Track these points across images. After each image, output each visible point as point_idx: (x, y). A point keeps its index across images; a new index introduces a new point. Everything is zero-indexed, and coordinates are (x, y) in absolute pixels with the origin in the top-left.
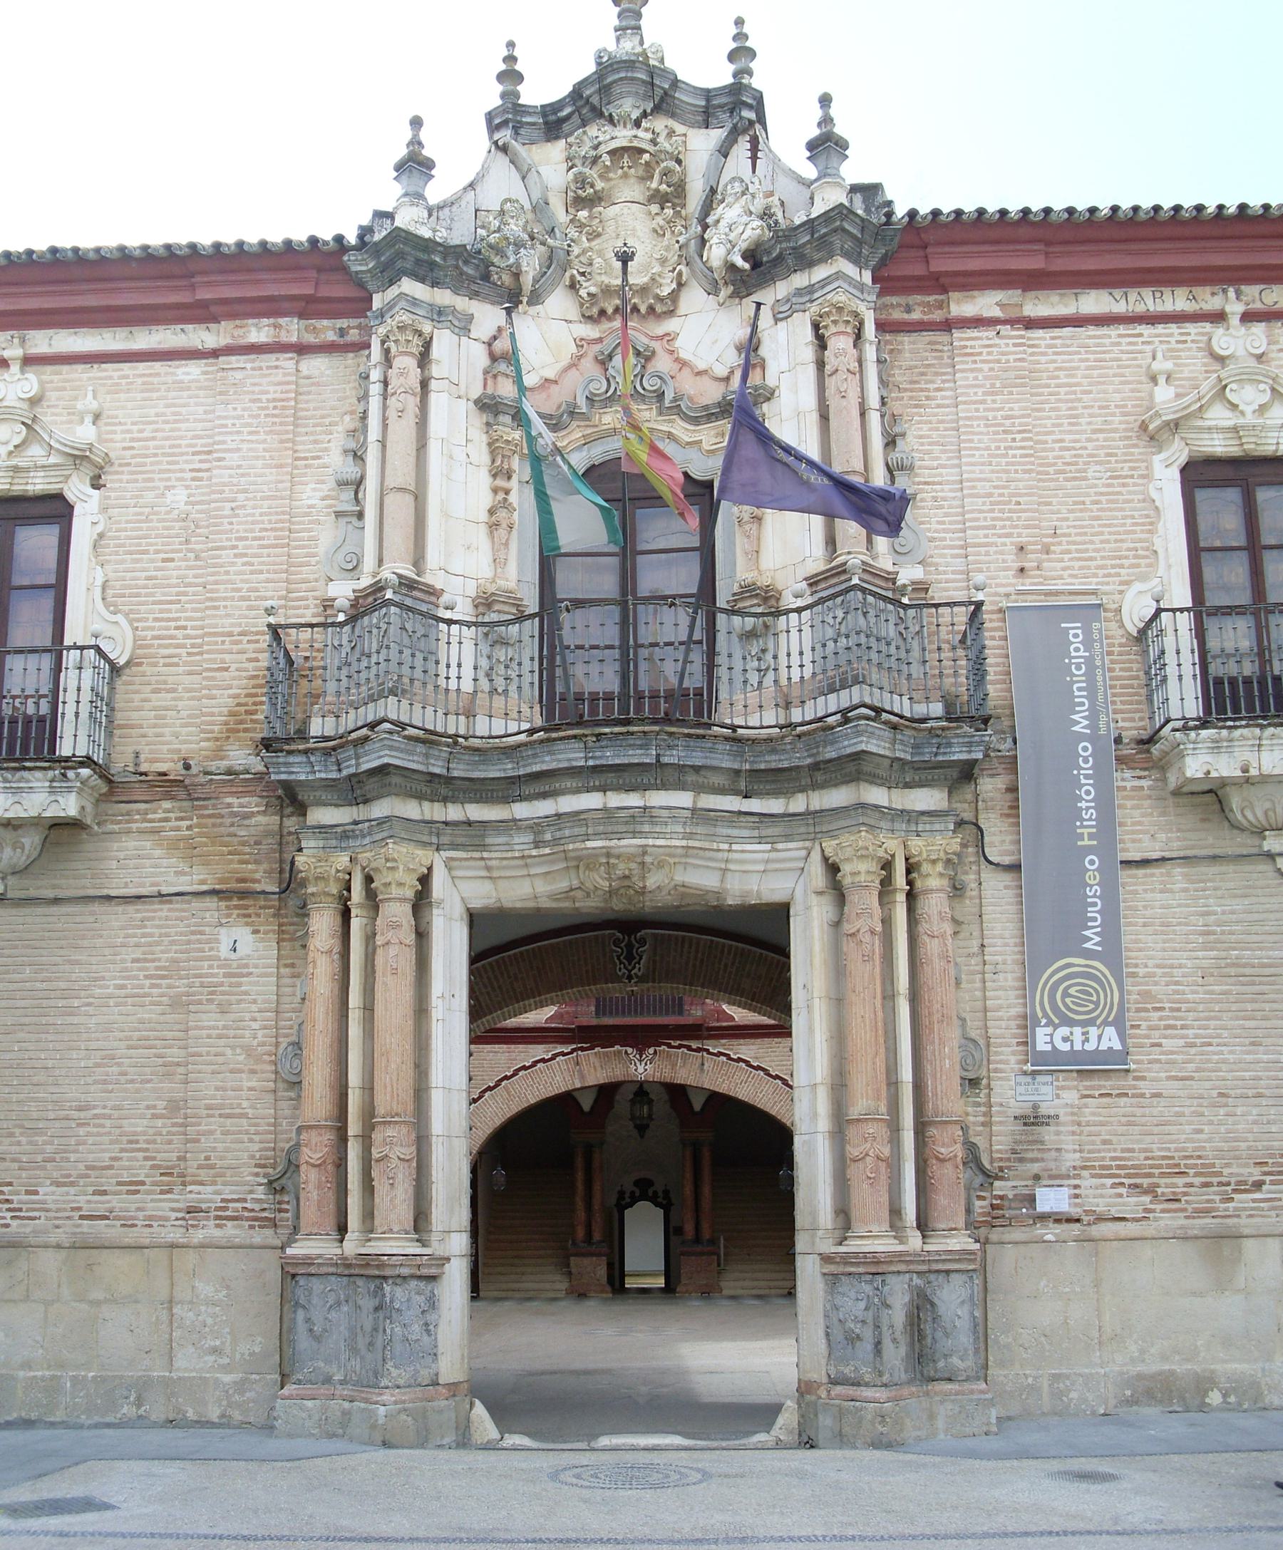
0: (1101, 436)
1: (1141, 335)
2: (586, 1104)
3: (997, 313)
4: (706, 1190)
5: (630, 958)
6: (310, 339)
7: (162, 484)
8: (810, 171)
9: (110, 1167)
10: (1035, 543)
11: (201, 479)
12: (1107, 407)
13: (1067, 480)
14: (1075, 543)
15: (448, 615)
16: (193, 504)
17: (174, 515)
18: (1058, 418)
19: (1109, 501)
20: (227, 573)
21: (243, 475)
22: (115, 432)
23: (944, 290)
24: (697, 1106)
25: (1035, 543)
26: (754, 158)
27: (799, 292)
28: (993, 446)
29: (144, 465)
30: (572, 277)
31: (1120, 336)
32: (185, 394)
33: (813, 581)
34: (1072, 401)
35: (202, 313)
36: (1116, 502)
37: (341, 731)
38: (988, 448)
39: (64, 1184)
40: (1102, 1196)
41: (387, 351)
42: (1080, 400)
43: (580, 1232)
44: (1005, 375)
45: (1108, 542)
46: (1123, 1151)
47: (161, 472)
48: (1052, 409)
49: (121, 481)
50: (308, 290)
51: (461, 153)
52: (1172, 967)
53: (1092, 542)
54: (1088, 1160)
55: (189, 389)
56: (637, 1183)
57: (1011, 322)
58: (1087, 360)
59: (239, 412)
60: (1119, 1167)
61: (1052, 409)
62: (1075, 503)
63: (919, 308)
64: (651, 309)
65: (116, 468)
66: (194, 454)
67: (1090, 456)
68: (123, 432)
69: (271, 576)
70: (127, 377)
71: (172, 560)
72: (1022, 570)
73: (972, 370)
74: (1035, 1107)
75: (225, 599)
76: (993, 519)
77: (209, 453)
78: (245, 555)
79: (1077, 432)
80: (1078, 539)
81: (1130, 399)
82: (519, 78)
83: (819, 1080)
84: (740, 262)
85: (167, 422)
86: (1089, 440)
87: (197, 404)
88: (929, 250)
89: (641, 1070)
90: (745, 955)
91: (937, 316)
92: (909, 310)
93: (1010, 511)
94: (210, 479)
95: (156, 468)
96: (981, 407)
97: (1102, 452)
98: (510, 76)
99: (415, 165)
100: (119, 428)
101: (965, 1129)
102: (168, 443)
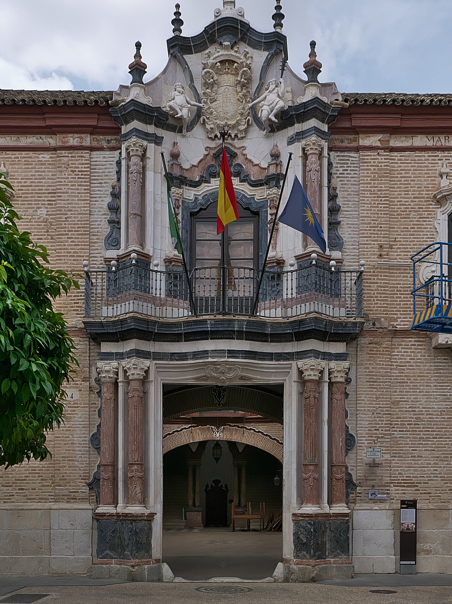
0: (417, 200)
1: (438, 156)
2: (194, 449)
3: (379, 144)
4: (243, 485)
5: (219, 397)
6: (95, 144)
7: (35, 206)
8: (305, 78)
9: (25, 480)
10: (386, 244)
11: (52, 204)
12: (421, 187)
13: (401, 218)
14: (402, 245)
15: (156, 269)
16: (49, 215)
17: (41, 220)
18: (400, 191)
19: (418, 228)
20: (65, 245)
21: (69, 204)
22: (14, 182)
23: (358, 133)
24: (240, 450)
25: (386, 244)
26: (283, 70)
27: (298, 134)
28: (373, 202)
29: (28, 197)
30: (204, 120)
31: (429, 156)
32: (43, 166)
33: (298, 258)
34: (406, 184)
35: (50, 131)
36: (421, 228)
37: (115, 315)
38: (370, 204)
39: (7, 486)
40: (398, 494)
41: (129, 153)
42: (410, 184)
43: (191, 502)
44: (380, 172)
45: (416, 245)
46: (406, 477)
47: (35, 201)
48: (398, 188)
49: (18, 204)
50: (95, 123)
51: (157, 60)
52: (429, 408)
53: (410, 245)
54: (393, 480)
55: (45, 164)
56: (214, 482)
57: (384, 149)
58: (414, 166)
59: (67, 176)
60: (404, 483)
61: (398, 188)
62: (404, 228)
63: (346, 140)
64: (236, 136)
65: (15, 198)
66: (48, 193)
67: (411, 208)
68: (18, 182)
69: (83, 247)
70: (18, 158)
71: (41, 239)
72: (381, 255)
73: (366, 170)
74: (374, 460)
75: (64, 256)
76: (370, 234)
77: (55, 193)
78: (72, 238)
79: (407, 198)
80: (404, 243)
81: (430, 184)
82: (181, 23)
83: (293, 450)
84: (274, 119)
85: (36, 179)
86: (412, 201)
87: (48, 171)
88: (352, 116)
89: (218, 435)
90: (267, 402)
91: (354, 144)
92: (342, 141)
93: (378, 230)
94: (55, 204)
95: (33, 199)
96: (369, 186)
97: (417, 207)
98: (177, 22)
99: (138, 69)
100: (16, 181)
101: (347, 468)
102: (37, 188)
